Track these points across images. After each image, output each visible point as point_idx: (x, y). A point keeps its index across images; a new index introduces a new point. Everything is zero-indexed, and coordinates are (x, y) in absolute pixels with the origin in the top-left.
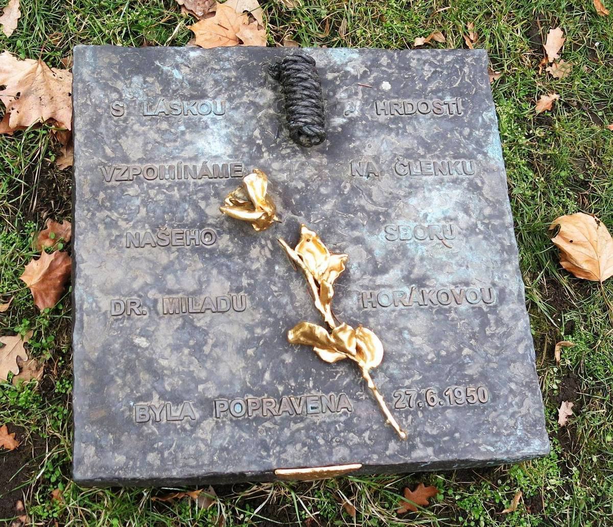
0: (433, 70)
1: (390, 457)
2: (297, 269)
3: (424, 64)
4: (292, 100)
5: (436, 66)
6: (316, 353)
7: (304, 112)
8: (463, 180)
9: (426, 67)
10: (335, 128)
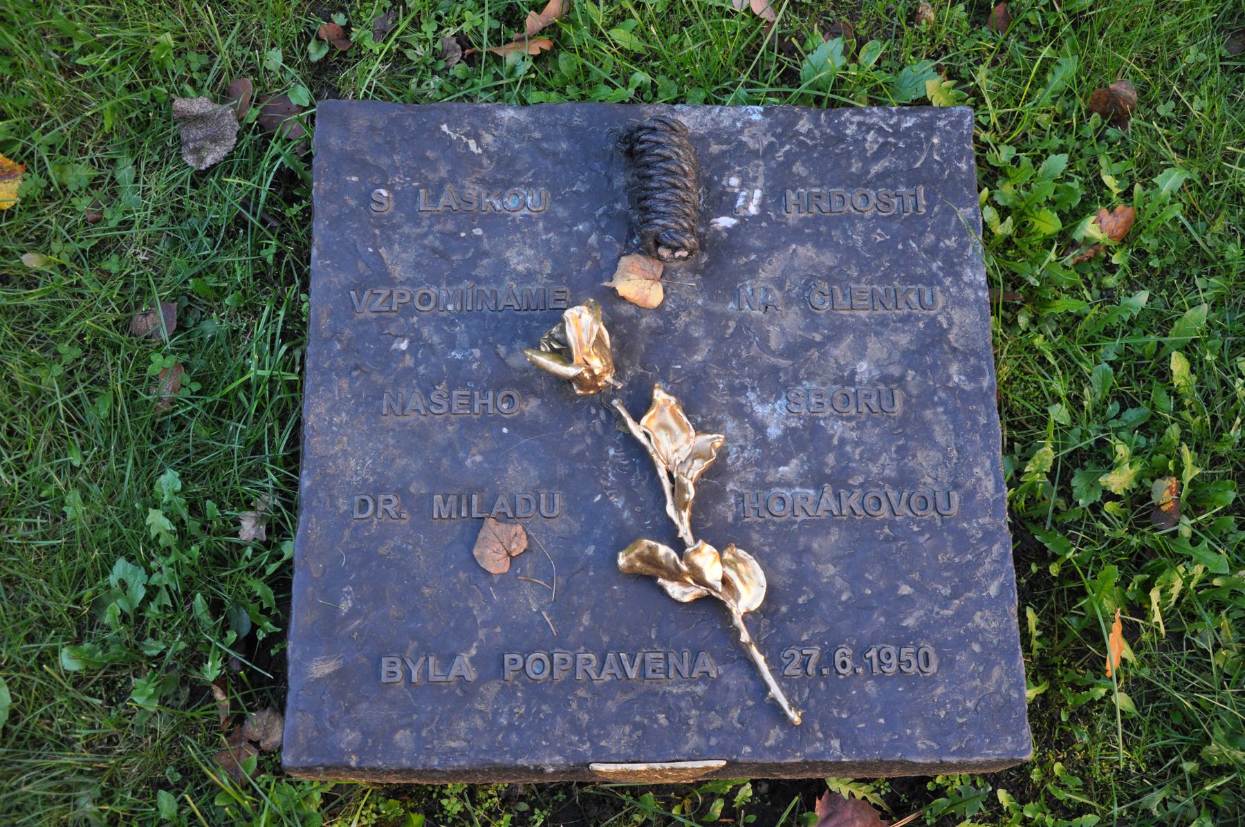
0: (881, 140)
1: (772, 750)
2: (640, 455)
3: (868, 132)
4: (647, 189)
5: (886, 134)
6: (662, 590)
7: (663, 209)
8: (918, 319)
9: (871, 136)
10: (717, 232)
